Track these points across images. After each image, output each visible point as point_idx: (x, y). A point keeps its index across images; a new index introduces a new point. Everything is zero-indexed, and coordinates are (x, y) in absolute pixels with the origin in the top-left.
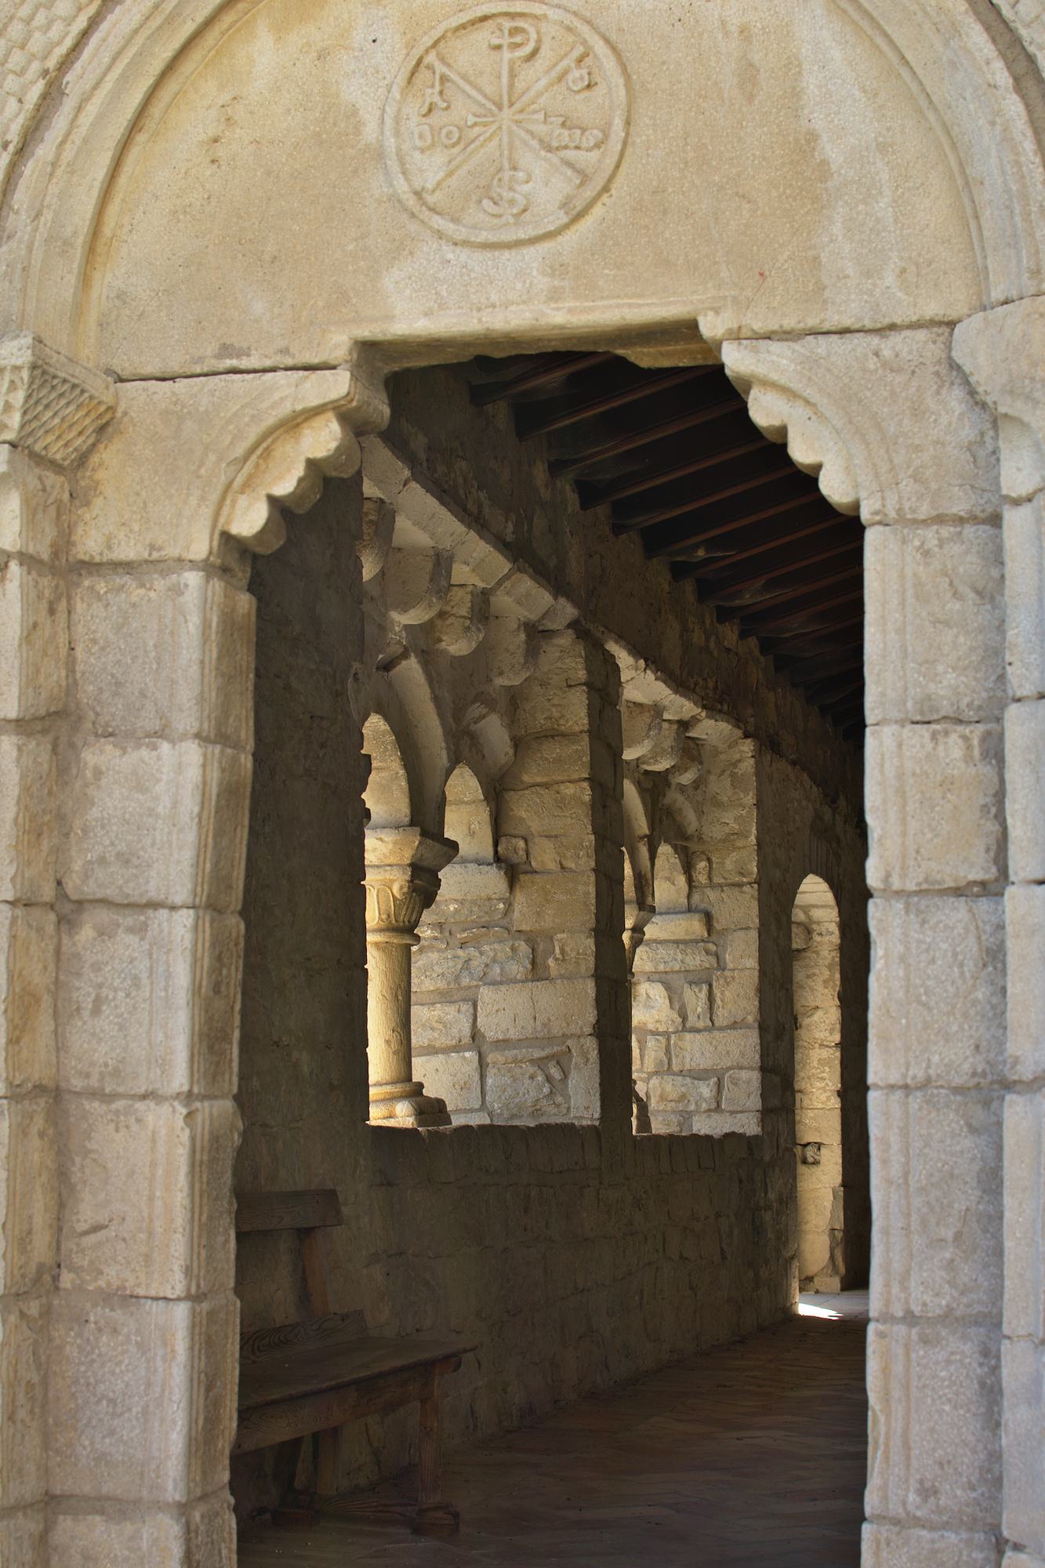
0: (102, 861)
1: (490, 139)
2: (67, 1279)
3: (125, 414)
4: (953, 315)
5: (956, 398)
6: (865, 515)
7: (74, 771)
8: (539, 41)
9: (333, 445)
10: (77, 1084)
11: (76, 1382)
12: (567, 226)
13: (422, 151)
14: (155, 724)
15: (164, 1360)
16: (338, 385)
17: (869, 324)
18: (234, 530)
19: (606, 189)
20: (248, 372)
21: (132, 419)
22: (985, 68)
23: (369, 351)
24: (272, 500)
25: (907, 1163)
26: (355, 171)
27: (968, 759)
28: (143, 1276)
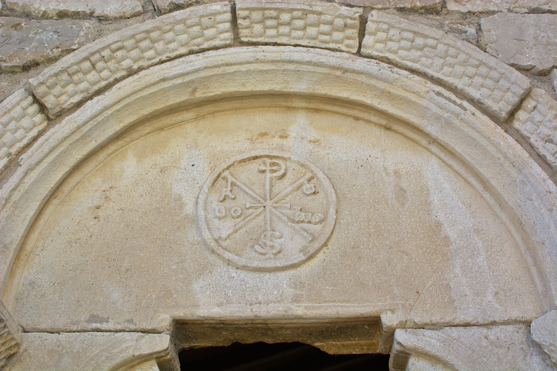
1: (258, 215)
3: (25, 350)
4: (527, 317)
8: (286, 170)
12: (304, 262)
13: (219, 218)
16: (163, 342)
17: (481, 321)
19: (325, 245)
20: (106, 331)
21: (30, 354)
22: (543, 183)
23: (181, 327)
26: (179, 228)
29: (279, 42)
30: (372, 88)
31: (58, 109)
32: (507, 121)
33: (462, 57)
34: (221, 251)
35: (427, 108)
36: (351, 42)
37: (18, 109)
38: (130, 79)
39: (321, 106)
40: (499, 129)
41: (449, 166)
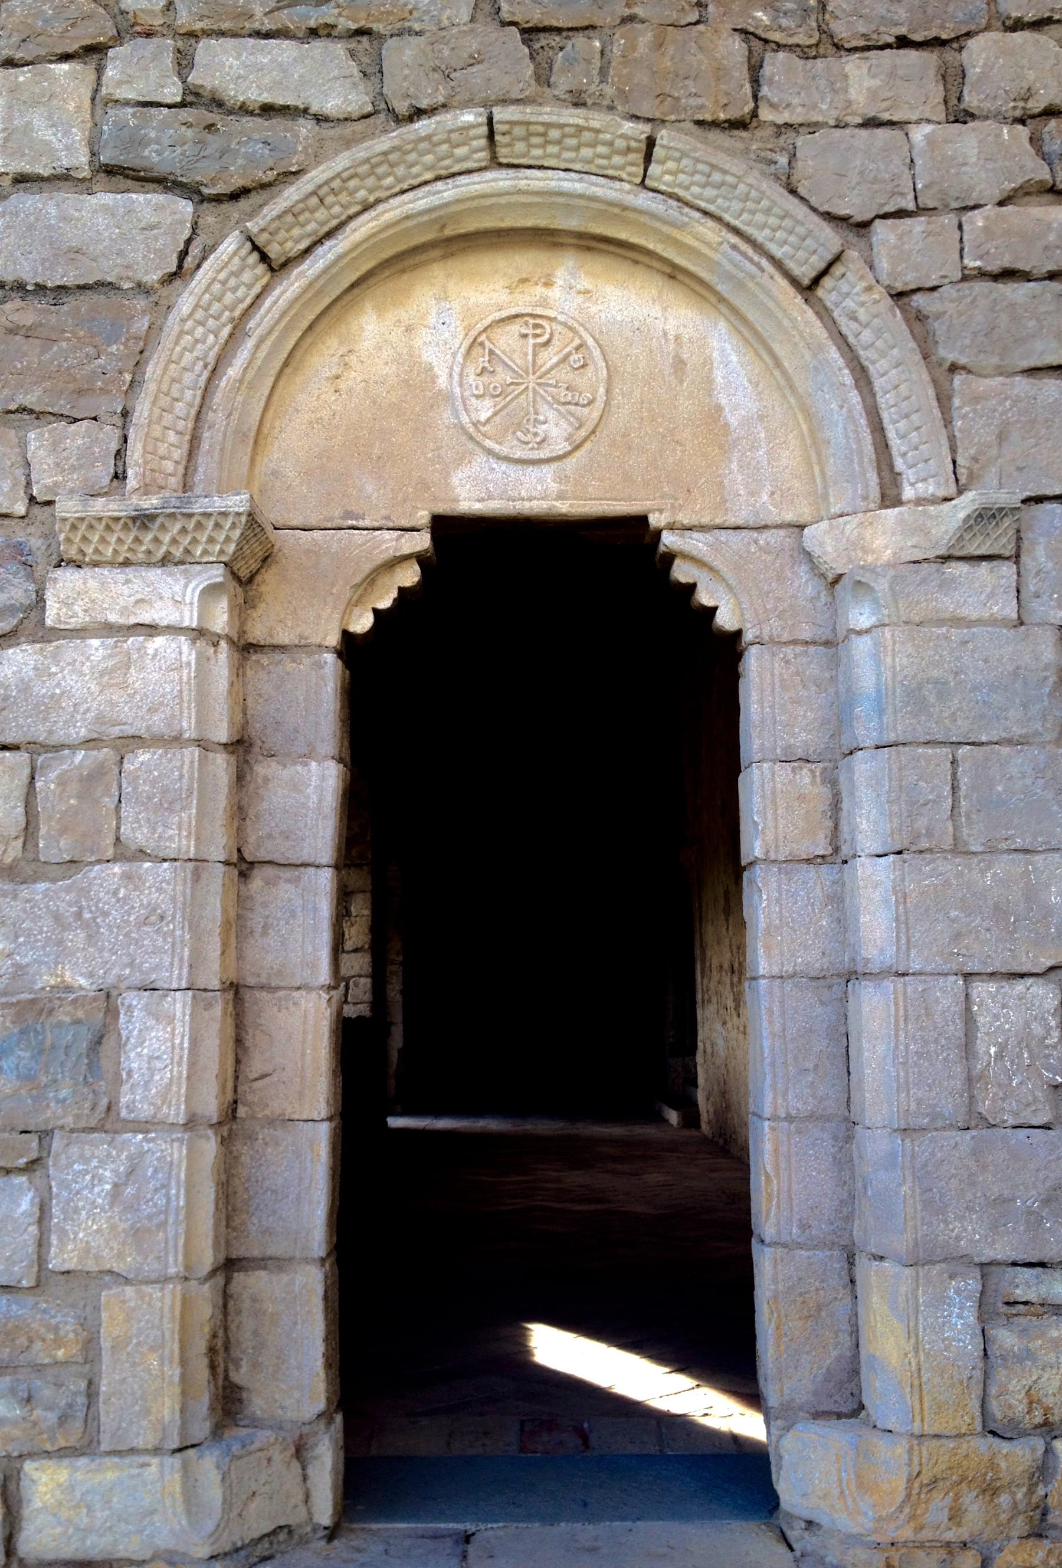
0: (270, 836)
2: (242, 1111)
5: (803, 570)
6: (748, 636)
7: (249, 778)
8: (551, 334)
9: (416, 579)
10: (251, 981)
11: (249, 1180)
14: (304, 750)
15: (312, 1161)
16: (422, 541)
17: (751, 523)
18: (351, 629)
24: (376, 611)
25: (784, 1024)
27: (813, 783)
28: (297, 1106)
29: (546, 164)
30: (656, 231)
31: (283, 259)
32: (809, 289)
33: (765, 203)
34: (480, 438)
35: (718, 263)
36: (633, 169)
37: (236, 260)
38: (366, 216)
39: (594, 244)
40: (799, 300)
41: (740, 332)
